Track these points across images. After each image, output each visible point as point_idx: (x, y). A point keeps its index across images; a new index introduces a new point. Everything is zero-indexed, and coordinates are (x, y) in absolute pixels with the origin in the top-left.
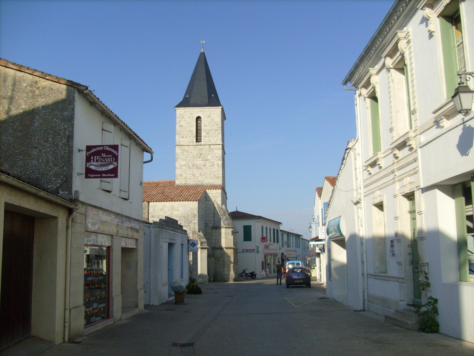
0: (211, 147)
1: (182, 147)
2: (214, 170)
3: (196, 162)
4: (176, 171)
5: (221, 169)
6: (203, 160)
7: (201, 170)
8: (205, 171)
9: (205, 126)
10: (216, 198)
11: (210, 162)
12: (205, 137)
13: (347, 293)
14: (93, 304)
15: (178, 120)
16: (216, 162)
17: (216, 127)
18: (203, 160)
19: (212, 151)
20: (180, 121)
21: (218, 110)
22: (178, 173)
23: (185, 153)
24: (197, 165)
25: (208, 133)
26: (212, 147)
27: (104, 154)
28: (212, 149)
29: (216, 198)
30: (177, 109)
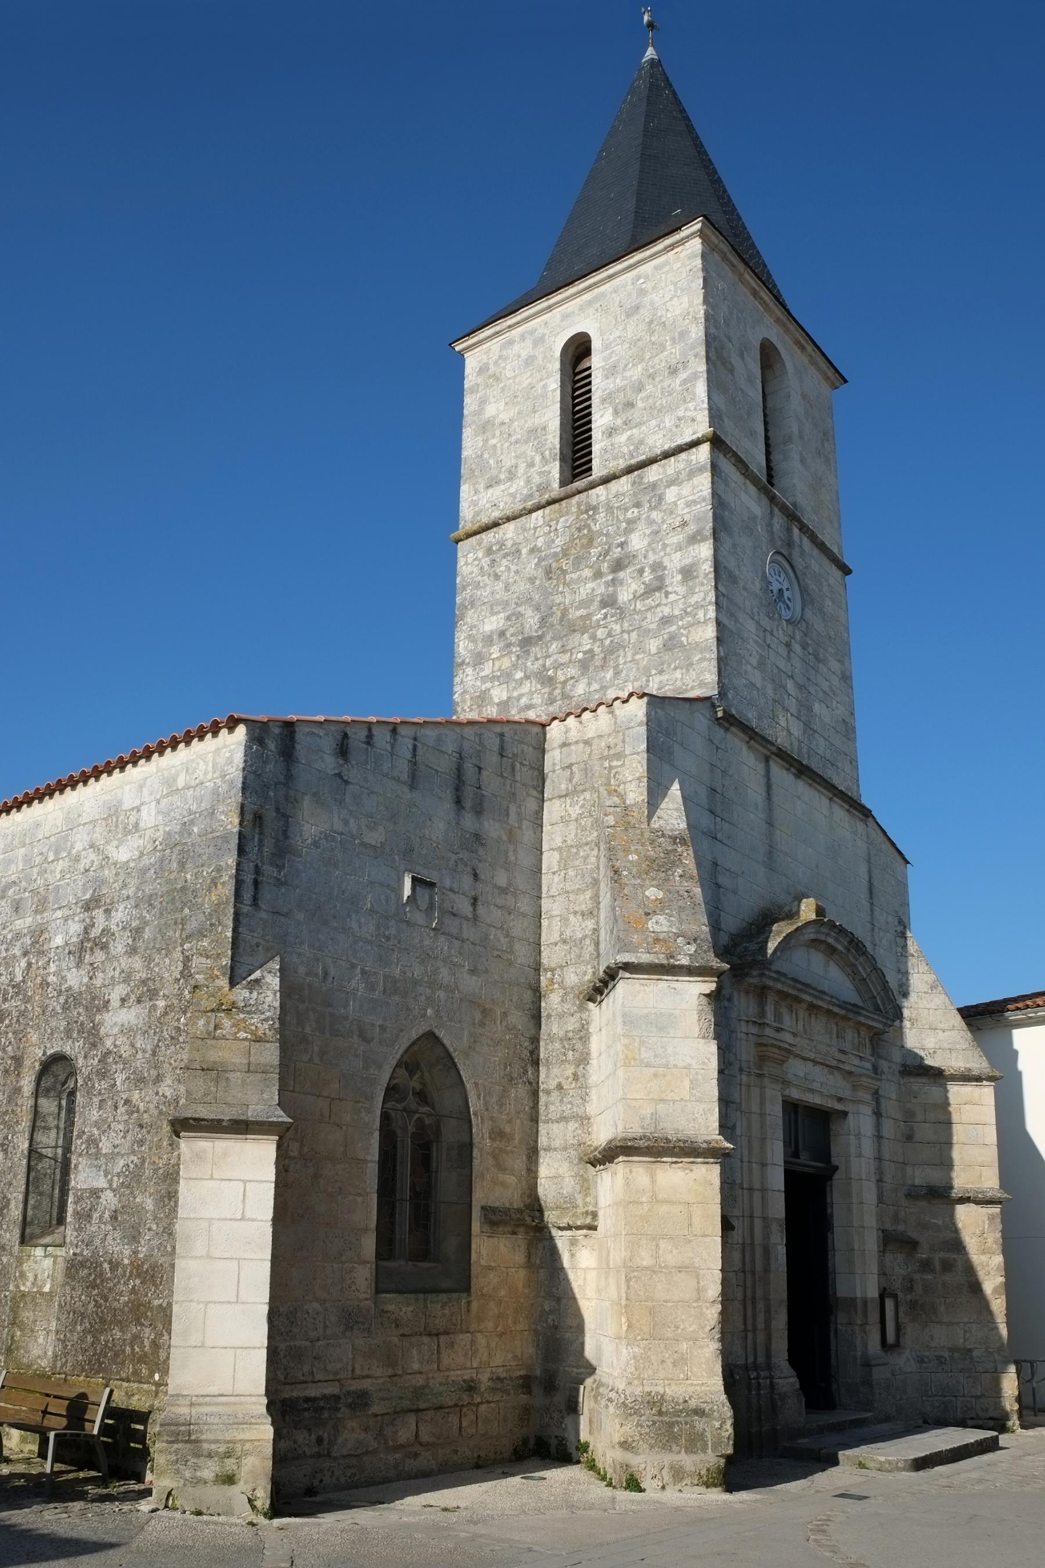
0: (646, 480)
1: (488, 537)
2: (667, 611)
3: (558, 599)
4: (457, 680)
5: (706, 594)
6: (598, 575)
7: (586, 636)
8: (609, 635)
9: (612, 371)
10: (615, 763)
11: (641, 571)
12: (611, 432)
13: (581, 745)
14: (993, 1084)
15: (470, 403)
16: (674, 561)
17: (673, 352)
18: (598, 575)
19: (649, 502)
20: (483, 402)
21: (682, 255)
22: (465, 692)
23: (505, 562)
24: (565, 612)
25: (630, 405)
26: (653, 473)
27: (812, 933)
28: (654, 486)
29: (615, 763)
30: (468, 348)
